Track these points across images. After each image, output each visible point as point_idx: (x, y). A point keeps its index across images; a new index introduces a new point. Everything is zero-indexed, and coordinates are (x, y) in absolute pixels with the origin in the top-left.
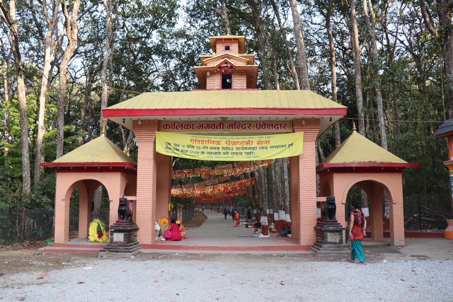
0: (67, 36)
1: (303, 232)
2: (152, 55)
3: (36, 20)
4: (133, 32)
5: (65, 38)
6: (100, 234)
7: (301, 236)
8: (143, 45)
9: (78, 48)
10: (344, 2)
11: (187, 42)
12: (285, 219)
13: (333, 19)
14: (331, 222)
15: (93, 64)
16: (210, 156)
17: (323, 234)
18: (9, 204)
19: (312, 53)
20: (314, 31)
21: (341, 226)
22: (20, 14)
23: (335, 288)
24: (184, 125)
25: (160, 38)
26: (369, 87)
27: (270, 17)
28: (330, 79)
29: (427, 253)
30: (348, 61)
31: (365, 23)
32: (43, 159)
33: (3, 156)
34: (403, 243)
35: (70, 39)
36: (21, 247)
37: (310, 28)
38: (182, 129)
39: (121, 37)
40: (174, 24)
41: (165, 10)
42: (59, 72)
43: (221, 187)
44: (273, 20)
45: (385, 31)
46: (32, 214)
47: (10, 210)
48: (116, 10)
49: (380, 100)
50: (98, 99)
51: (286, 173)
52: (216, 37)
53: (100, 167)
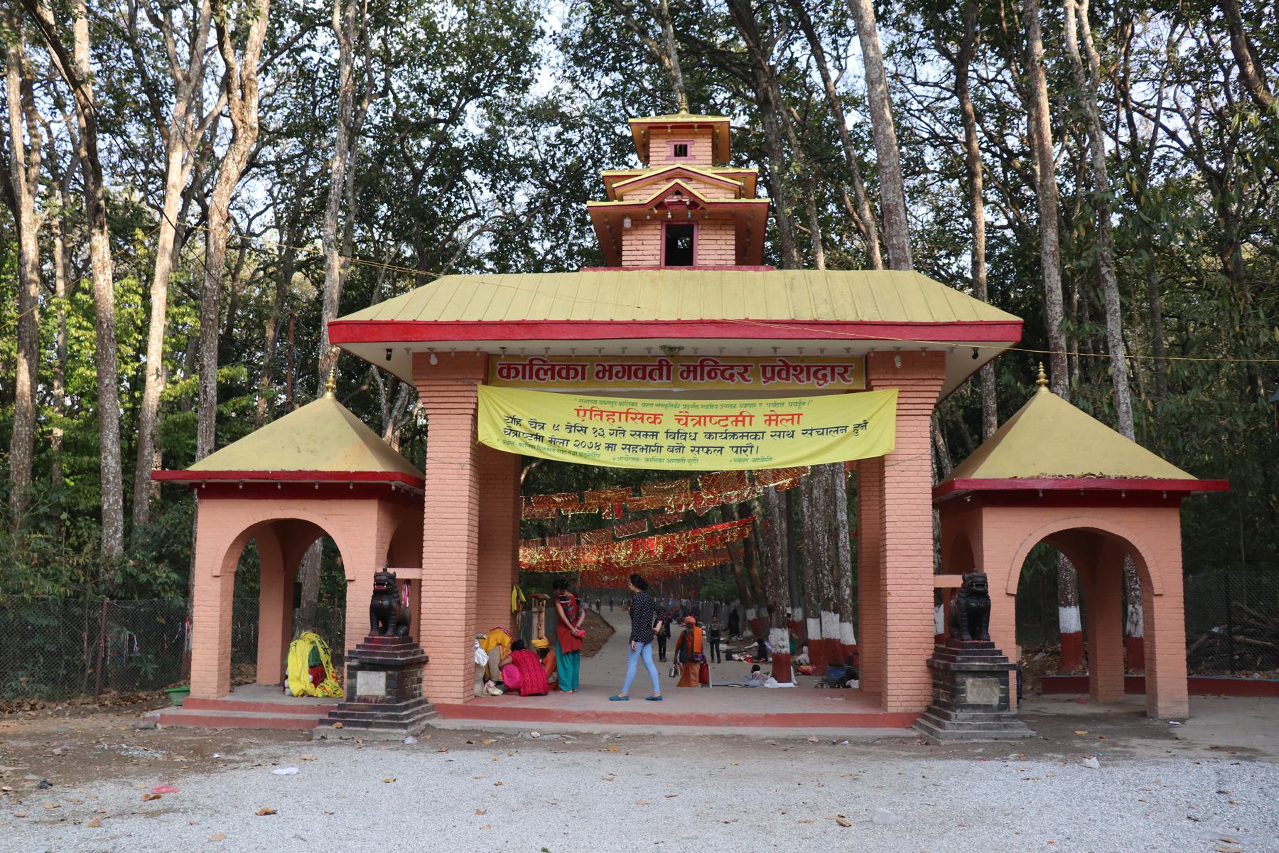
0: (230, 117)
1: (894, 674)
2: (465, 169)
3: (143, 75)
4: (413, 105)
5: (225, 123)
6: (318, 674)
7: (889, 687)
8: (439, 143)
9: (258, 150)
10: (1008, 22)
11: (562, 133)
12: (838, 637)
13: (975, 71)
14: (976, 645)
15: (300, 194)
16: (631, 455)
17: (954, 682)
18: (64, 585)
19: (915, 166)
20: (920, 102)
21: (1006, 659)
22: (99, 57)
23: (995, 838)
24: (557, 368)
25: (487, 124)
26: (1083, 263)
27: (798, 65)
28: (966, 240)
29: (1258, 741)
30: (1017, 188)
31: (1071, 78)
32: (157, 460)
33: (49, 451)
34: (1184, 710)
35: (239, 124)
36: (96, 706)
37: (909, 96)
38: (553, 378)
39: (377, 121)
40: (527, 83)
41: (501, 44)
42: (205, 216)
43: (657, 546)
44: (805, 74)
45: (1125, 105)
46: (126, 614)
47: (66, 602)
48: (366, 45)
49: (1113, 298)
50: (313, 293)
51: (842, 505)
52: (647, 120)
53: (320, 485)
